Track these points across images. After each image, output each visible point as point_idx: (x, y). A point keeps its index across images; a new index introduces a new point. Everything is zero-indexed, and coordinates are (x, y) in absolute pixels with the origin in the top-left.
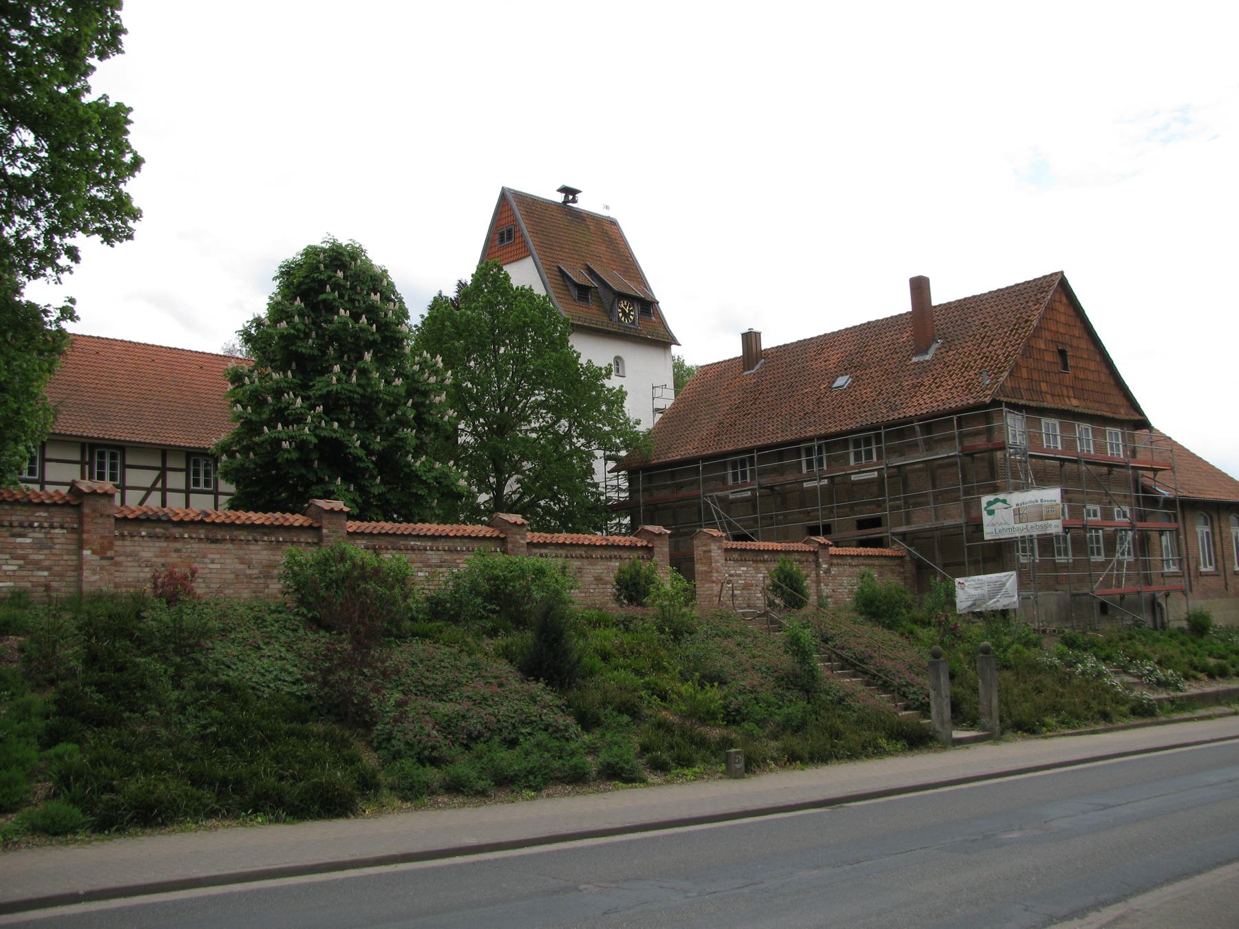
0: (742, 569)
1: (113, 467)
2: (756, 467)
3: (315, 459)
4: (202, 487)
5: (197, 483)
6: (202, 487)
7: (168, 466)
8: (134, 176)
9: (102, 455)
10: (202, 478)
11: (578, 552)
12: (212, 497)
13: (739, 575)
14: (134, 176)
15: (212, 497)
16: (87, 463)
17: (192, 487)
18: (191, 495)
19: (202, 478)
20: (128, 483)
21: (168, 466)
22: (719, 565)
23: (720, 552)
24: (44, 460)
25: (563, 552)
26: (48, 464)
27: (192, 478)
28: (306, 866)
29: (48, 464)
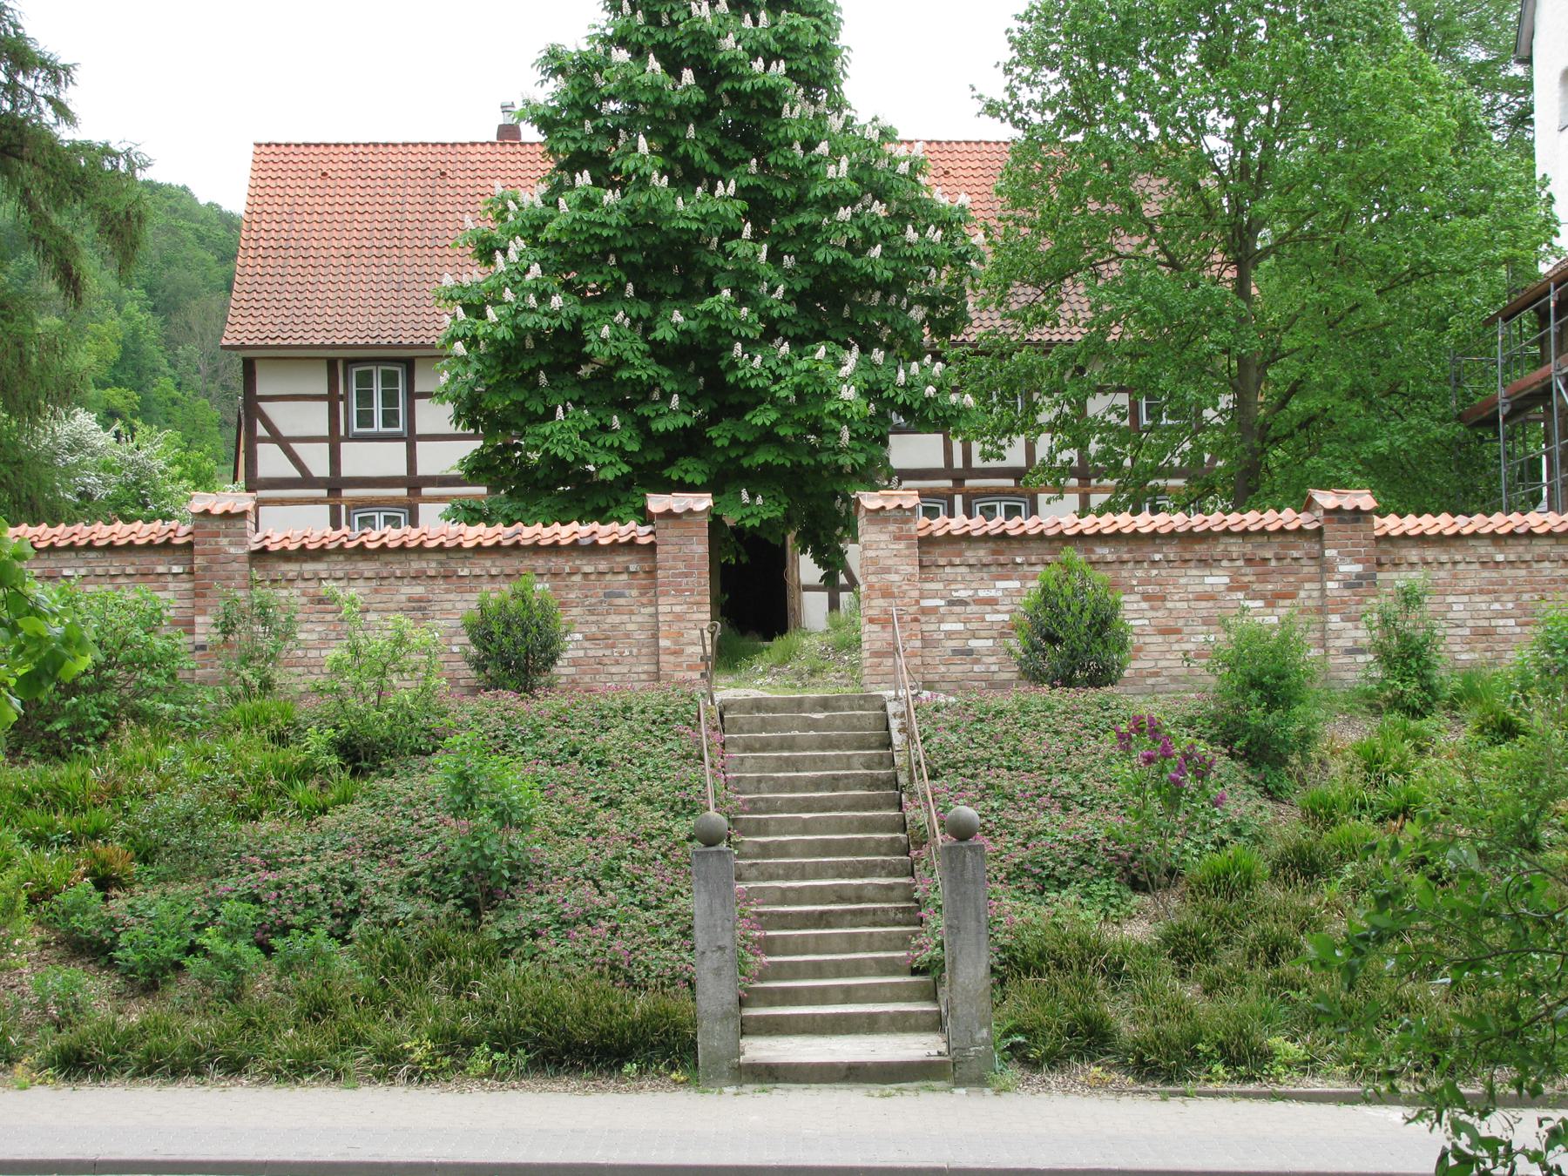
0: (1001, 584)
1: (390, 399)
2: (1556, 446)
3: (672, 393)
4: (378, 427)
5: (365, 419)
6: (378, 427)
7: (259, 392)
8: (555, 63)
9: (365, 380)
10: (378, 409)
11: (416, 565)
12: (401, 447)
13: (991, 602)
14: (555, 63)
15: (401, 447)
16: (342, 398)
17: (356, 429)
18: (419, 444)
19: (378, 409)
20: (420, 429)
21: (259, 392)
22: (894, 577)
23: (902, 545)
24: (412, 396)
25: (368, 568)
26: (419, 403)
27: (355, 409)
28: (876, 1089)
29: (419, 403)
